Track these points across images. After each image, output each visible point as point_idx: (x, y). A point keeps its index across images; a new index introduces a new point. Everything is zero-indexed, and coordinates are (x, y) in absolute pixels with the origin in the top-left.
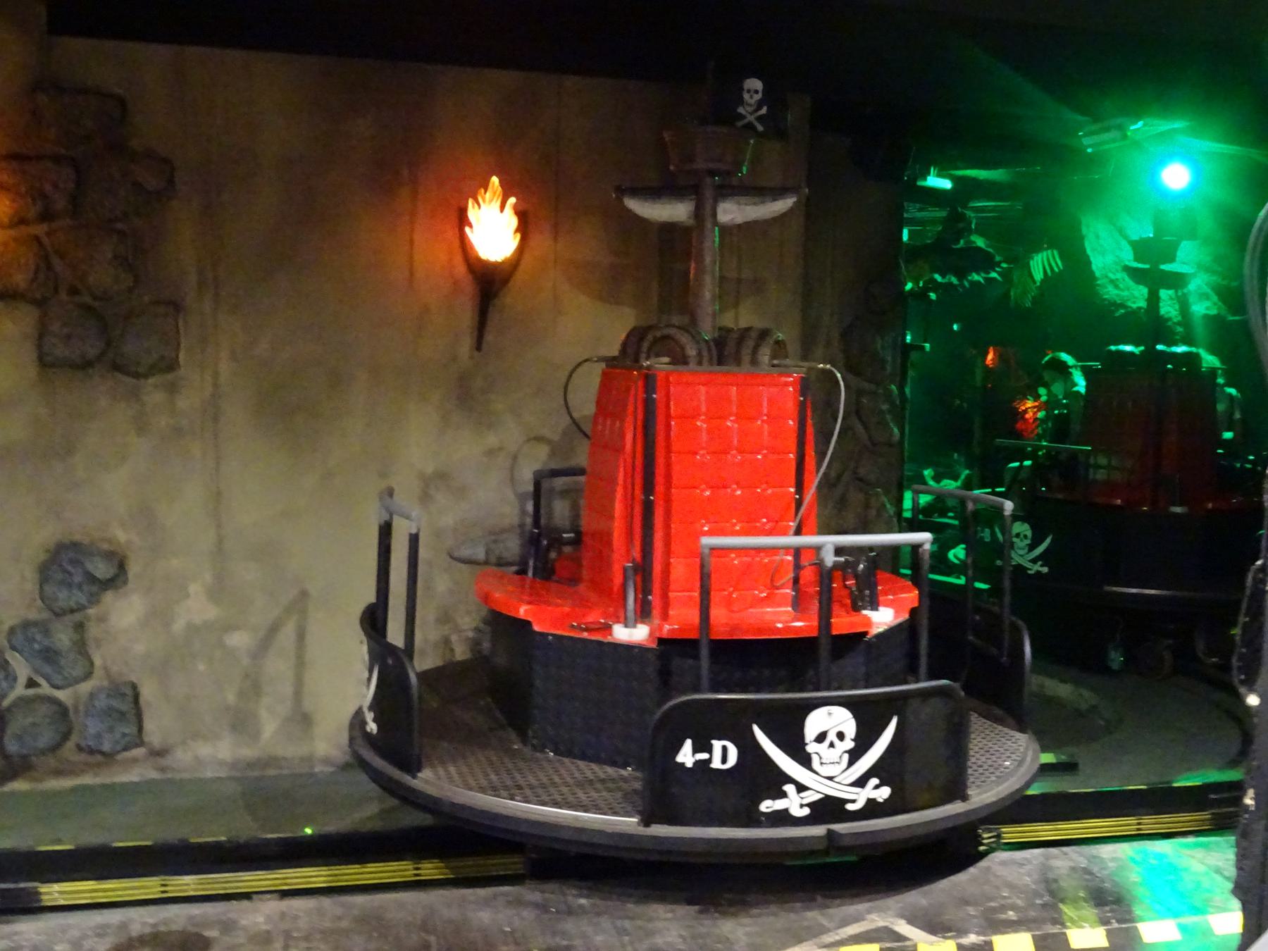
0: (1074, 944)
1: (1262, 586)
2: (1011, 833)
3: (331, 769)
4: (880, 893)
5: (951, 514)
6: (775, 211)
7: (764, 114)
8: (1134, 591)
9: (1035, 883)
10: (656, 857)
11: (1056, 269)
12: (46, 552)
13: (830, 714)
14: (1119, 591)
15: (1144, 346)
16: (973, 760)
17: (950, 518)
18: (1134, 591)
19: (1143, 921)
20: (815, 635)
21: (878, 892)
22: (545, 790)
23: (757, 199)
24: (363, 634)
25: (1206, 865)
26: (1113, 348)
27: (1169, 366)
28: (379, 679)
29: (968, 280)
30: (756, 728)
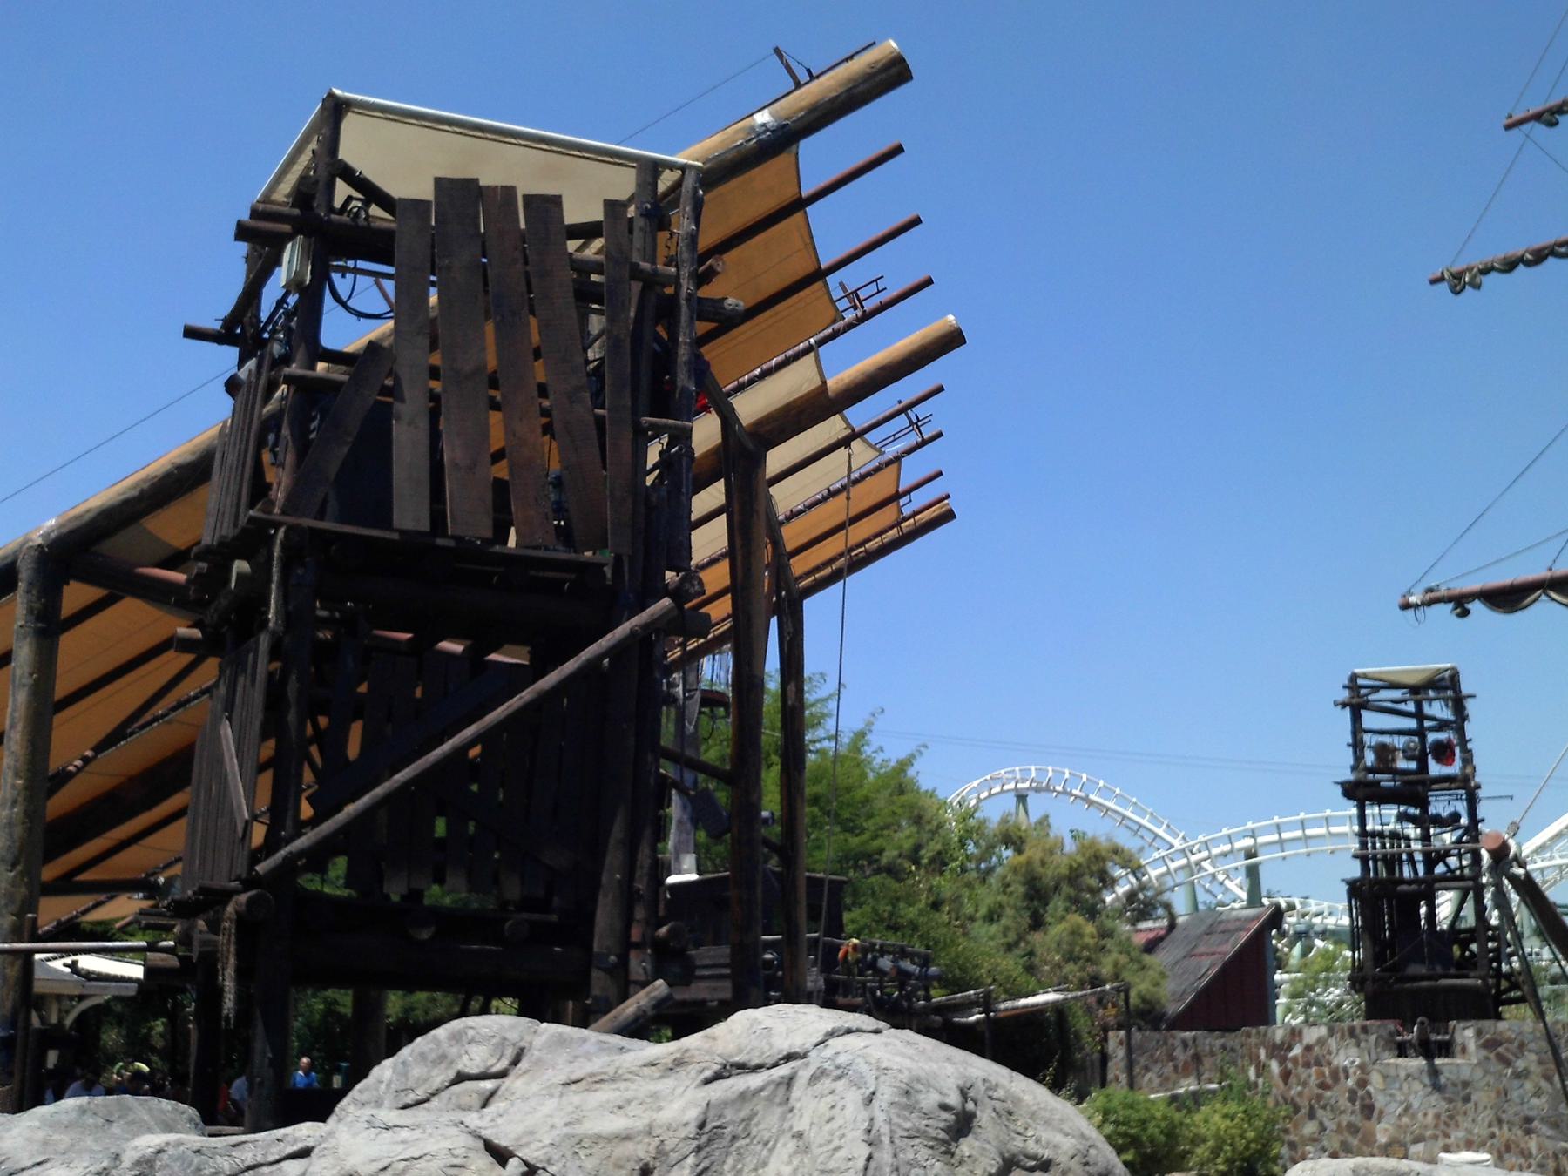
0: (261, 872)
1: (1446, 936)
2: (1443, 884)
3: (392, 338)
4: (286, 500)
5: (475, 752)
6: (842, 380)
7: (397, 287)
8: (401, 777)
9: (1023, 902)
10: (662, 823)
11: (727, 971)
12: (1354, 1171)
13: (900, 402)
14: (659, 608)
15: (357, 761)
16: (1254, 1031)
17: (472, 743)
18: (401, 777)
19: (1406, 1057)
20: (395, 522)
21: (72, 532)
22: (1503, 1149)
23: (105, 506)
24: (215, 345)
25: (1338, 1050)
26: (957, 1019)
27: (418, 693)
28: (512, 664)
29: (175, 999)
30: (774, 621)
